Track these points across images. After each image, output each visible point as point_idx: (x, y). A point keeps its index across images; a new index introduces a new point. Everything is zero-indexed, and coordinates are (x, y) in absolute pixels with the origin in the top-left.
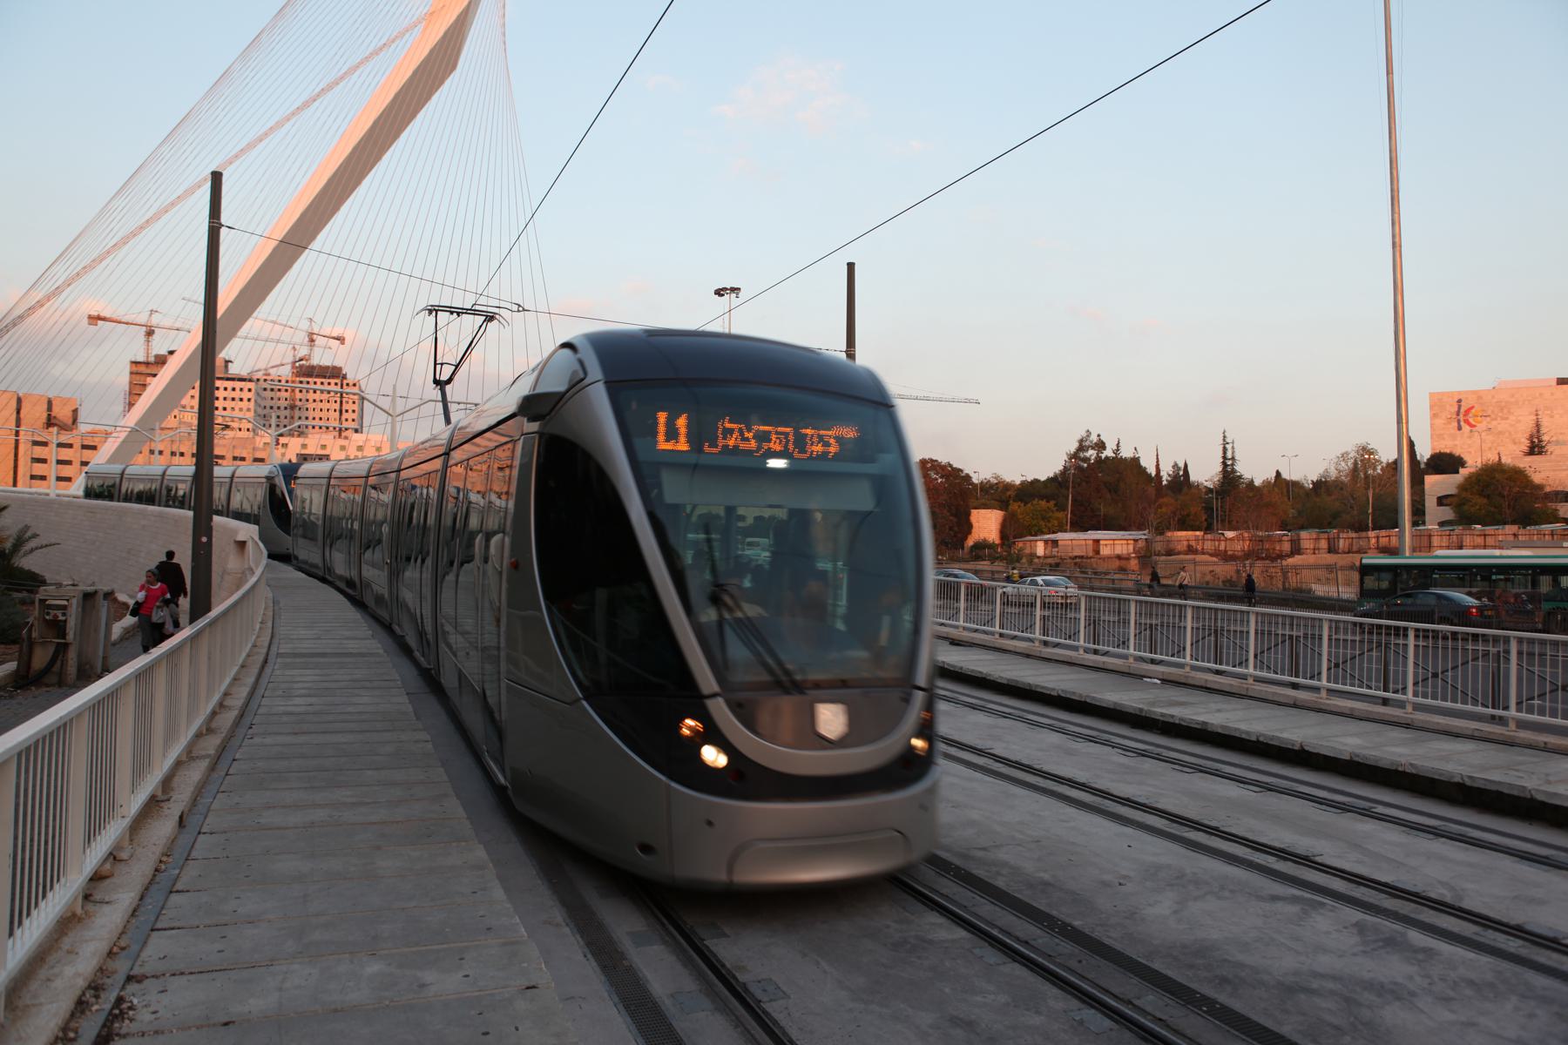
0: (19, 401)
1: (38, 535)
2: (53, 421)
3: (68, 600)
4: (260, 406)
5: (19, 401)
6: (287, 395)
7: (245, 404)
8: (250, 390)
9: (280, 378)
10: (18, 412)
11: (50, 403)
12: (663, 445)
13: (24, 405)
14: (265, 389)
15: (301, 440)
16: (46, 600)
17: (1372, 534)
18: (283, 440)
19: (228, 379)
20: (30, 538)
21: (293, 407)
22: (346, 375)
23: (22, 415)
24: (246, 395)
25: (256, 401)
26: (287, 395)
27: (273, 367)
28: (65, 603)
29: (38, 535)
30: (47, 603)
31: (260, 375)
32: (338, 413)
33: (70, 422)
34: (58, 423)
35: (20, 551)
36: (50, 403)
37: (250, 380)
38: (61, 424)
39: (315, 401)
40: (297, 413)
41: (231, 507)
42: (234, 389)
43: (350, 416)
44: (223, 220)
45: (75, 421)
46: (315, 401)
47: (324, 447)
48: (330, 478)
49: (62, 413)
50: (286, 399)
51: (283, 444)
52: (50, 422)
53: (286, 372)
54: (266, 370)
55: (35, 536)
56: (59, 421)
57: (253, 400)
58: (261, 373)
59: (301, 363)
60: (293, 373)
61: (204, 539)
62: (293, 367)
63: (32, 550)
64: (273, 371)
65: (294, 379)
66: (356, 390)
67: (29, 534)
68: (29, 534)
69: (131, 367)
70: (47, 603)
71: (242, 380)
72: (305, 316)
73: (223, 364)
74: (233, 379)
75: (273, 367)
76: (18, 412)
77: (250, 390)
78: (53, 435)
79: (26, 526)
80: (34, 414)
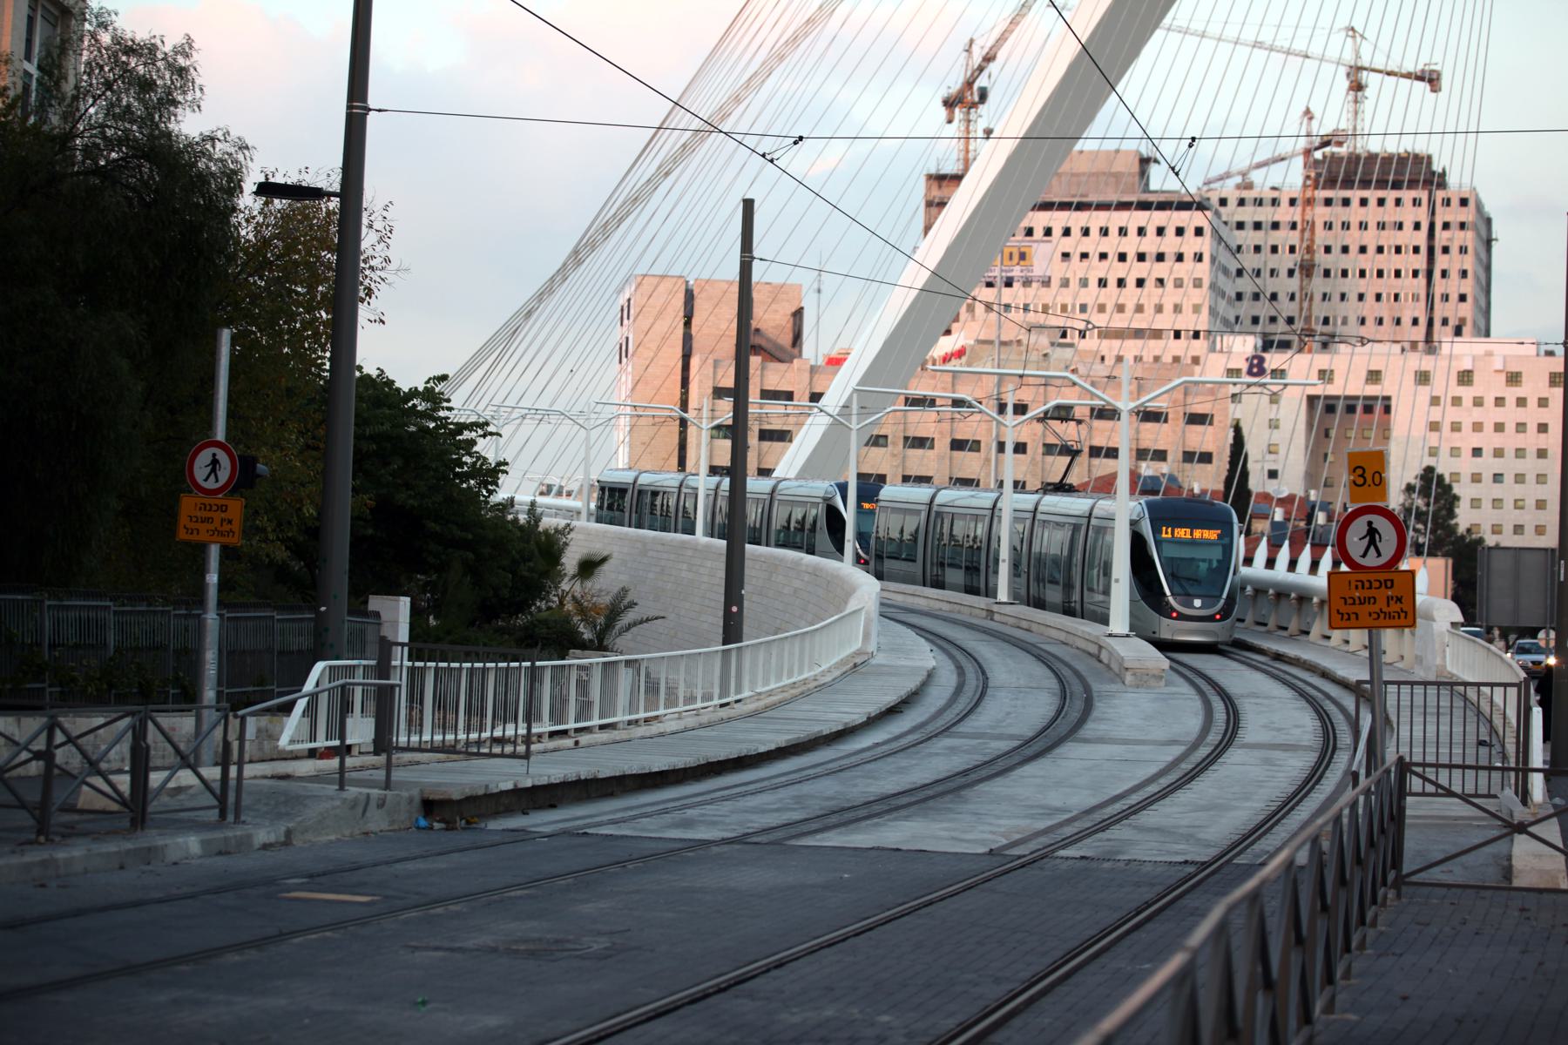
0: (689, 297)
1: (636, 604)
2: (755, 340)
4: (1226, 271)
5: (689, 297)
6: (1294, 238)
7: (1187, 269)
8: (1199, 232)
9: (1275, 194)
10: (688, 324)
12: (1164, 535)
13: (698, 303)
14: (1240, 226)
15: (1322, 360)
18: (1273, 360)
19: (1144, 206)
20: (626, 608)
21: (1307, 269)
22: (1443, 175)
24: (1190, 245)
25: (1213, 259)
26: (1294, 238)
27: (1259, 166)
29: (636, 604)
31: (1229, 189)
32: (1422, 279)
33: (786, 339)
34: (764, 343)
35: (614, 627)
37: (1201, 206)
38: (773, 351)
39: (1363, 250)
40: (1318, 284)
41: (1033, 550)
42: (1141, 231)
43: (1454, 286)
44: (756, 254)
45: (797, 338)
46: (1380, 250)
47: (1374, 376)
48: (1090, 517)
50: (1292, 249)
51: (1273, 371)
53: (1292, 177)
54: (1244, 175)
55: (632, 605)
56: (768, 340)
57: (1206, 258)
58: (1231, 183)
59: (1327, 150)
60: (1308, 177)
61: (1175, 615)
62: (1311, 164)
63: (629, 627)
64: (1257, 177)
65: (1309, 194)
66: (1467, 215)
67: (626, 602)
68: (626, 602)
69: (929, 189)
71: (1184, 206)
72: (1336, 26)
73: (1136, 168)
74: (1163, 206)
75: (1259, 166)
76: (688, 324)
77: (1199, 232)
79: (623, 589)
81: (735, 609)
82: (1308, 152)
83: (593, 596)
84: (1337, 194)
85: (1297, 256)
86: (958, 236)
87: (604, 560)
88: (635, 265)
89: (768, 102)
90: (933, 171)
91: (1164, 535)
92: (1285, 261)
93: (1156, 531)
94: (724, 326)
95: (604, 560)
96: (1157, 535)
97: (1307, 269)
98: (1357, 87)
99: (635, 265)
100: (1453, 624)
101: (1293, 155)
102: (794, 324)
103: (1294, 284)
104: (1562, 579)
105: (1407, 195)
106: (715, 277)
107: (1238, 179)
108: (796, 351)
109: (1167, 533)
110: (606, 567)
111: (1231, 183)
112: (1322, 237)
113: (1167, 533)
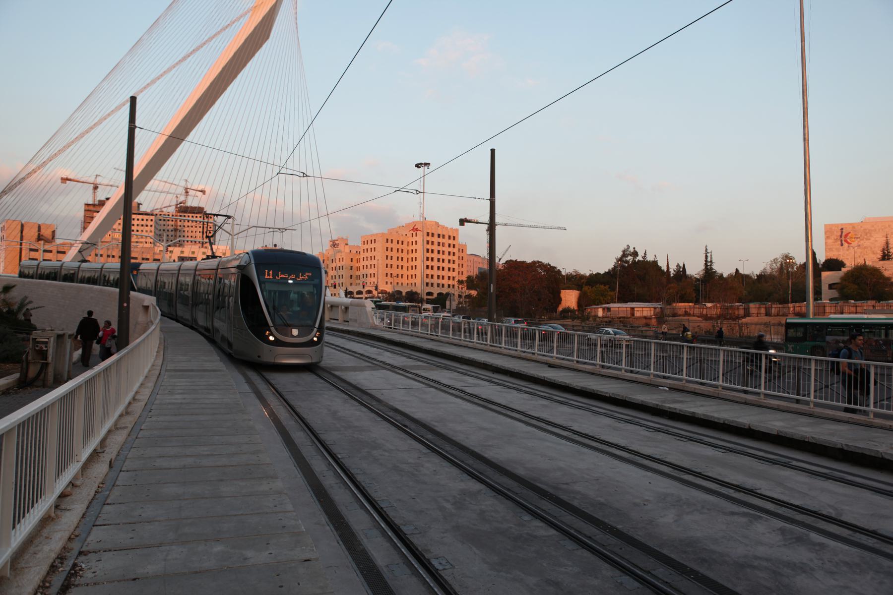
0: (22, 226)
1: (32, 302)
2: (41, 237)
3: (48, 339)
4: (157, 229)
6: (173, 223)
7: (149, 228)
8: (152, 220)
10: (22, 232)
11: (39, 227)
14: (160, 220)
15: (180, 249)
16: (36, 338)
17: (791, 305)
18: (170, 249)
19: (140, 214)
21: (176, 230)
23: (24, 234)
24: (149, 223)
26: (173, 223)
27: (165, 207)
28: (47, 340)
29: (32, 302)
30: (37, 340)
31: (157, 212)
32: (201, 233)
33: (50, 238)
34: (43, 238)
36: (39, 227)
37: (152, 215)
45: (53, 237)
47: (193, 253)
49: (46, 233)
50: (172, 226)
51: (170, 251)
52: (39, 238)
53: (172, 210)
54: (161, 209)
55: (30, 302)
58: (158, 211)
64: (164, 210)
67: (27, 301)
68: (27, 301)
69: (85, 207)
70: (37, 340)
73: (137, 206)
75: (165, 207)
76: (22, 232)
77: (152, 220)
78: (41, 246)
80: (31, 234)
81: (125, 305)
82: (177, 205)
83: (10, 299)
84: (183, 214)
85: (173, 227)
86: (140, 193)
87: (14, 286)
88: (6, 216)
89: (18, 209)
90: (86, 203)
91: (266, 277)
92: (171, 228)
93: (260, 274)
94: (32, 234)
95: (14, 286)
96: (261, 277)
97: (176, 230)
98: (187, 192)
99: (6, 216)
100: (372, 308)
101: (173, 205)
102: (53, 234)
103: (173, 233)
104: (492, 291)
105: (199, 215)
106: (30, 221)
107: (160, 210)
108: (53, 240)
109: (269, 275)
110: (14, 289)
111: (158, 211)
112: (179, 223)
113: (269, 275)
